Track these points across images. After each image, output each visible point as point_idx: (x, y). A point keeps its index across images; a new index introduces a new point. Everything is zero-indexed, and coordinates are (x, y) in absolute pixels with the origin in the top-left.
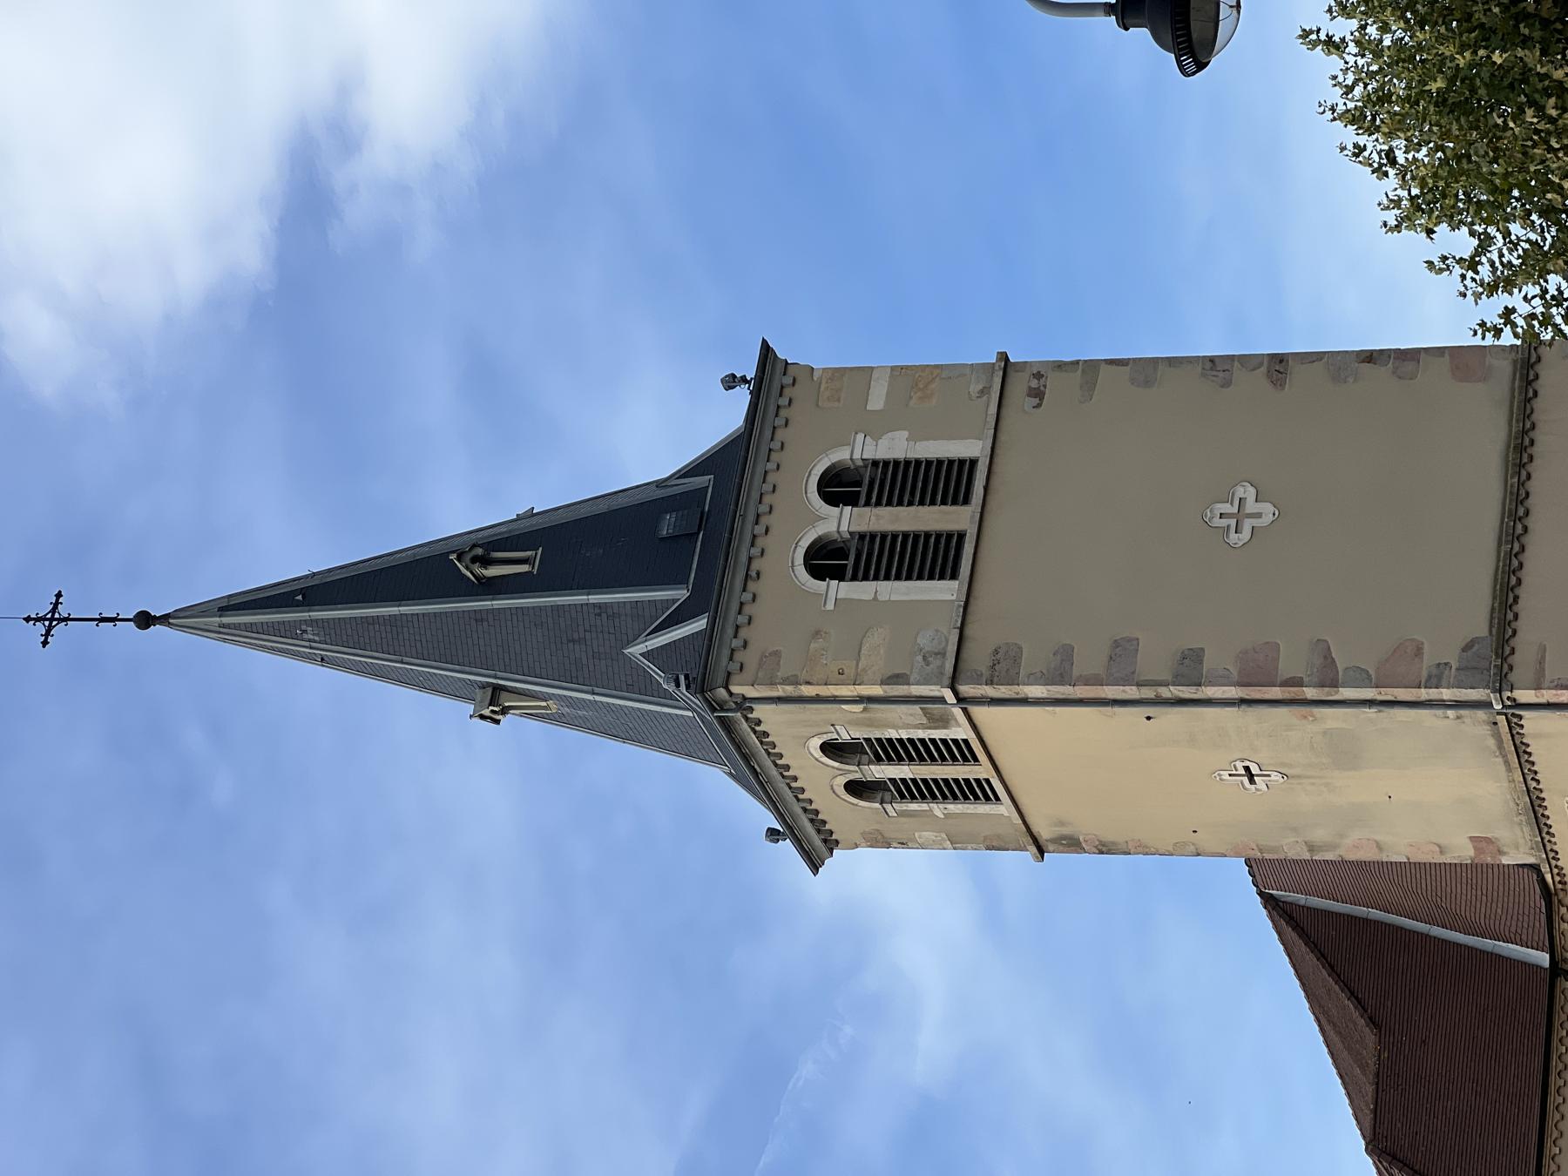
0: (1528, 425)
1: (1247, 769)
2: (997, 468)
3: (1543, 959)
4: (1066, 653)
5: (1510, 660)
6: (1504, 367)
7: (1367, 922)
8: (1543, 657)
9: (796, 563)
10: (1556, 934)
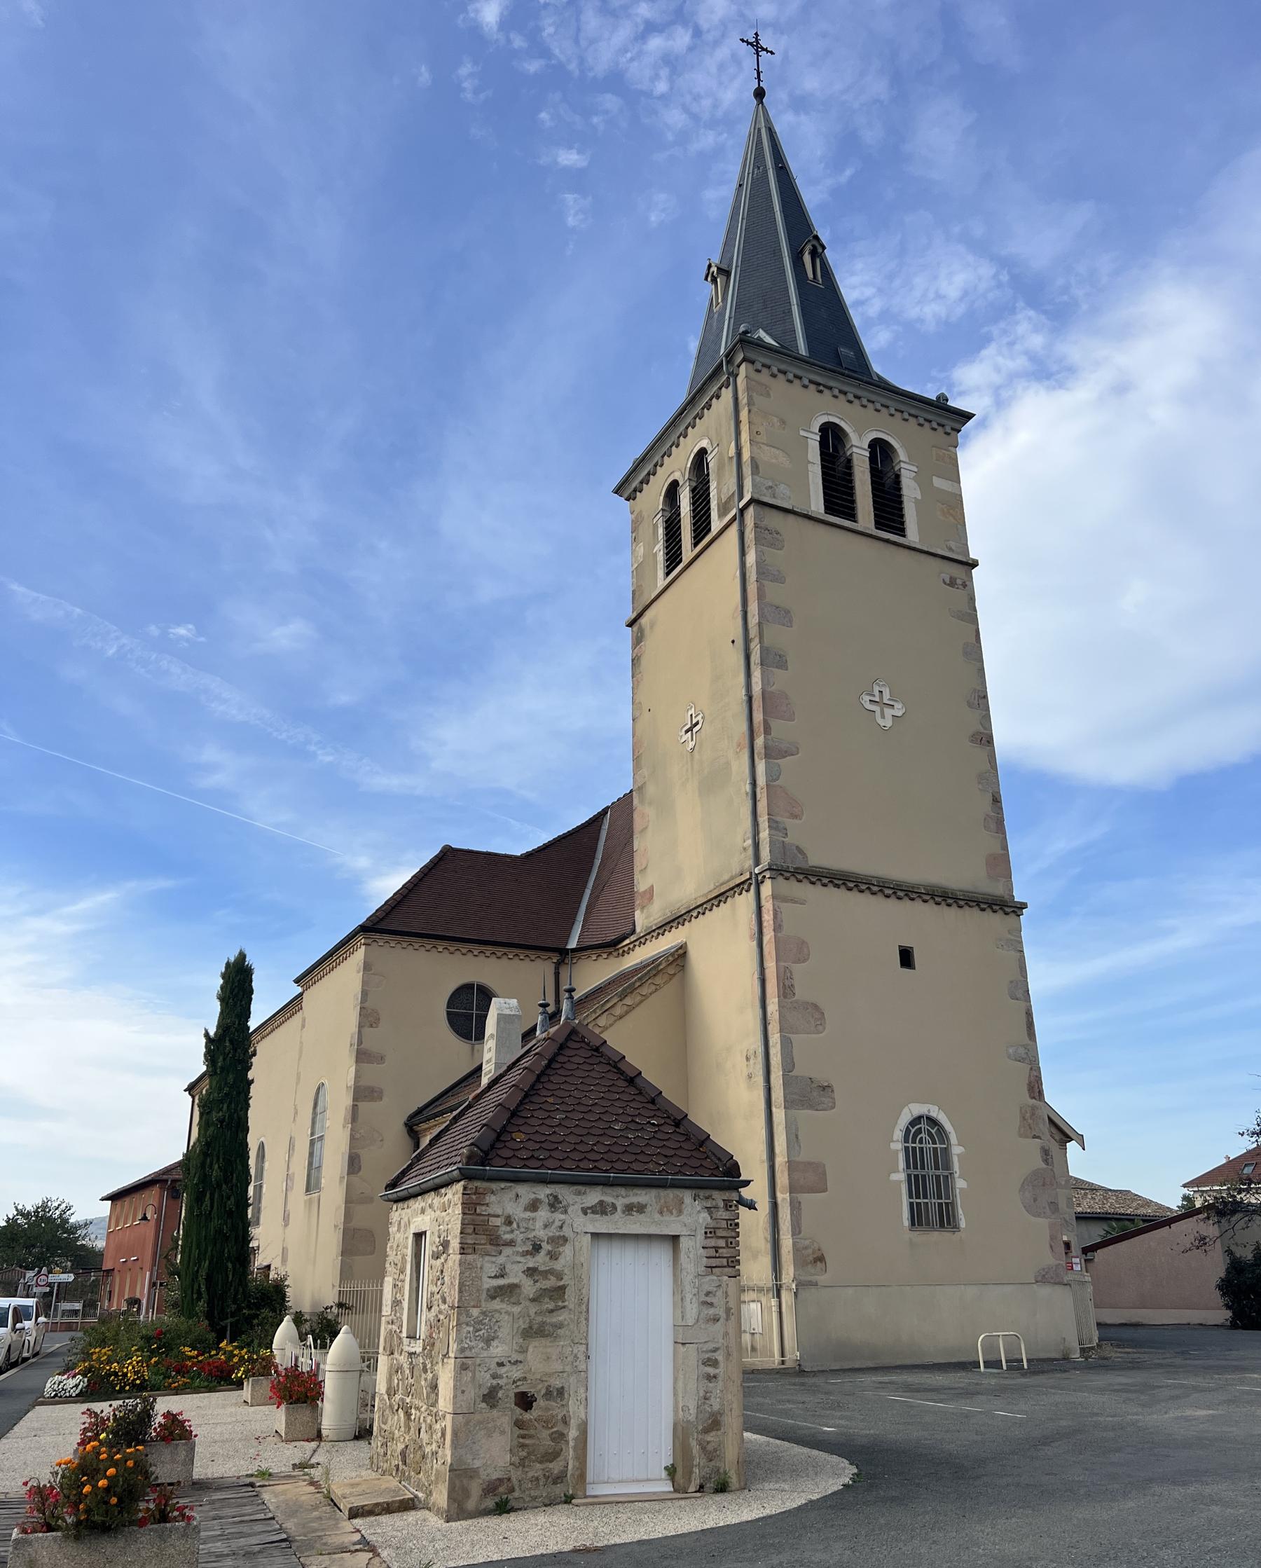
0: (962, 903)
1: (697, 723)
2: (901, 550)
3: (573, 944)
4: (779, 579)
5: (792, 878)
6: (998, 890)
7: (593, 857)
8: (796, 902)
9: (830, 417)
10: (589, 952)
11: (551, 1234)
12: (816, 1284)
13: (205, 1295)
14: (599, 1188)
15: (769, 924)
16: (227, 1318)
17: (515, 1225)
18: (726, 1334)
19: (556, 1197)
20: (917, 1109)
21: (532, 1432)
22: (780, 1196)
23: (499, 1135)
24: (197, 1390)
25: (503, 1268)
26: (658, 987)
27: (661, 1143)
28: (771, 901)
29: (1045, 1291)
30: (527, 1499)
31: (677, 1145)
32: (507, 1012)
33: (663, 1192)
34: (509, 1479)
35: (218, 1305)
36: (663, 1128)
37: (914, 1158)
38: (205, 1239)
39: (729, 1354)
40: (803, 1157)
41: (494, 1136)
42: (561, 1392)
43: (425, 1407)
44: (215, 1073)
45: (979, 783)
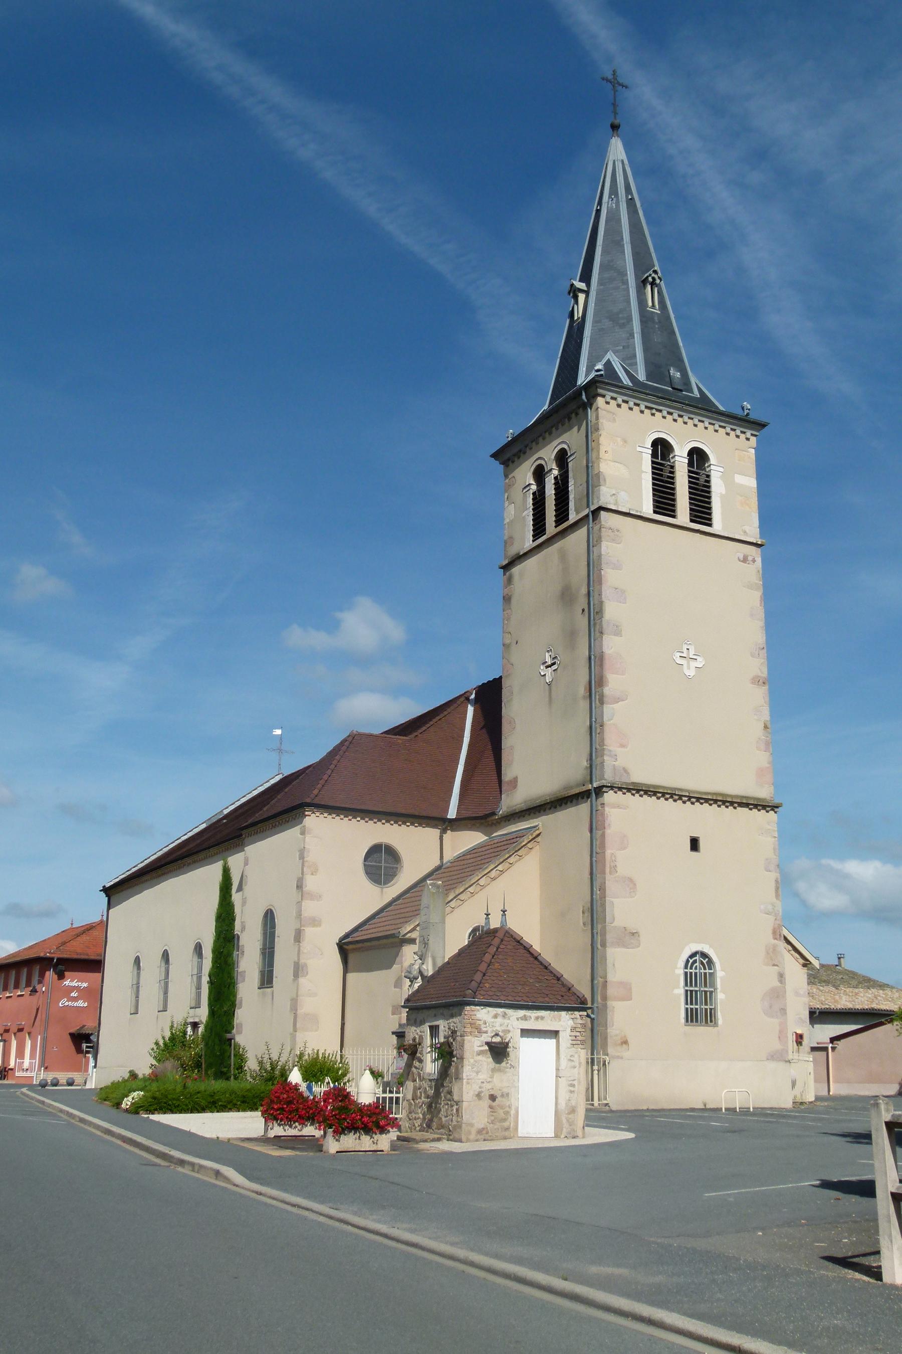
11: (503, 1029)
12: (622, 1058)
17: (488, 1024)
20: (695, 948)
21: (496, 1111)
26: (521, 858)
29: (772, 1065)
30: (494, 1136)
34: (487, 1128)
37: (689, 979)
42: (508, 1094)
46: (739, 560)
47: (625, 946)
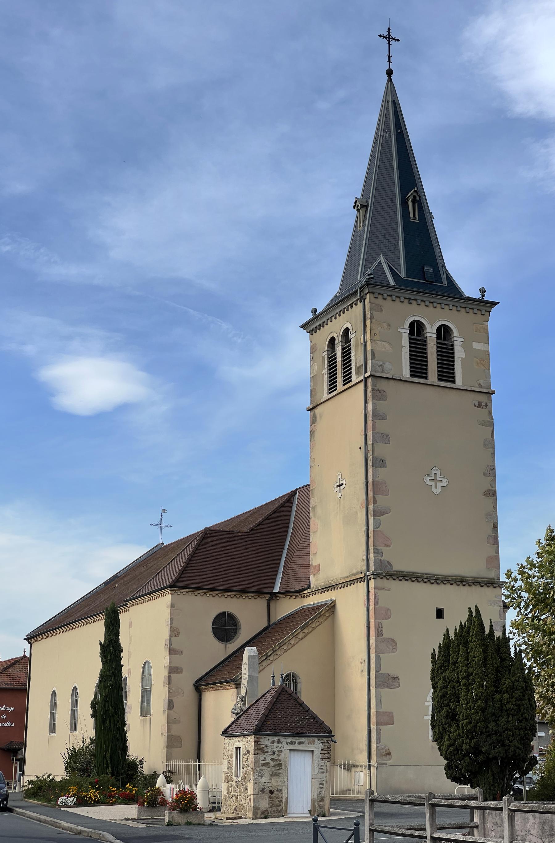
0: (470, 584)
1: (342, 484)
3: (276, 590)
7: (288, 527)
8: (386, 590)
13: (110, 765)
14: (291, 738)
15: (372, 601)
16: (120, 776)
17: (268, 747)
18: (326, 776)
19: (279, 740)
21: (273, 800)
22: (372, 726)
23: (263, 723)
24: (120, 804)
25: (265, 758)
26: (320, 623)
27: (309, 724)
28: (373, 590)
31: (314, 725)
32: (252, 654)
33: (309, 738)
34: (268, 811)
35: (115, 770)
36: (310, 720)
38: (108, 740)
39: (327, 782)
40: (382, 710)
41: (262, 723)
42: (281, 790)
43: (243, 794)
44: (106, 662)
45: (486, 518)
46: (475, 406)
47: (388, 687)
